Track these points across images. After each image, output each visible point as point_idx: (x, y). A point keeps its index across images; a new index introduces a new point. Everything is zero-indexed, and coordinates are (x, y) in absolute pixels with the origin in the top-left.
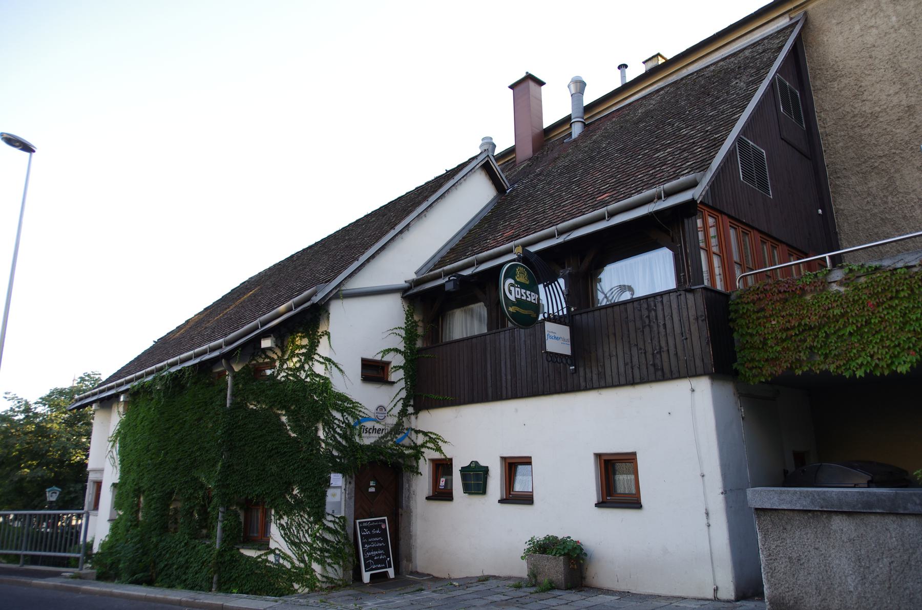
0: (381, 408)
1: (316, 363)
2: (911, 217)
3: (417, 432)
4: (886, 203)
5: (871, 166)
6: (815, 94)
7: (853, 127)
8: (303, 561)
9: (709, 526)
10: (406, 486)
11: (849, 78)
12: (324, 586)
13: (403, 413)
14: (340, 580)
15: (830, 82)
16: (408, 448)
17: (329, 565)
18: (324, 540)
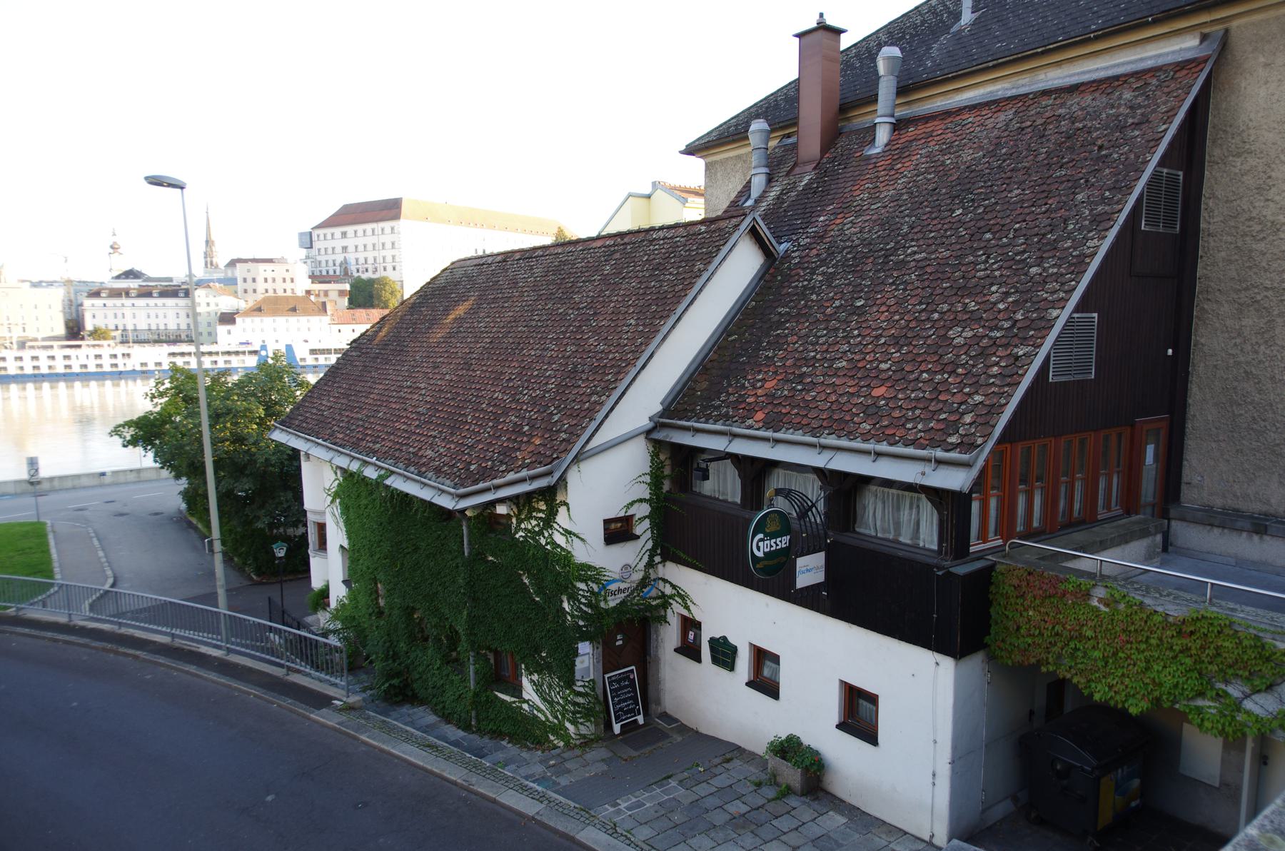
0: (626, 566)
1: (555, 532)
2: (1280, 380)
3: (665, 581)
4: (1256, 352)
5: (1253, 298)
6: (1209, 168)
7: (1245, 235)
8: (556, 717)
9: (934, 784)
10: (654, 637)
11: (1259, 158)
12: (578, 742)
13: (650, 564)
14: (593, 734)
15: (1234, 156)
16: (655, 599)
17: (581, 724)
18: (575, 704)
